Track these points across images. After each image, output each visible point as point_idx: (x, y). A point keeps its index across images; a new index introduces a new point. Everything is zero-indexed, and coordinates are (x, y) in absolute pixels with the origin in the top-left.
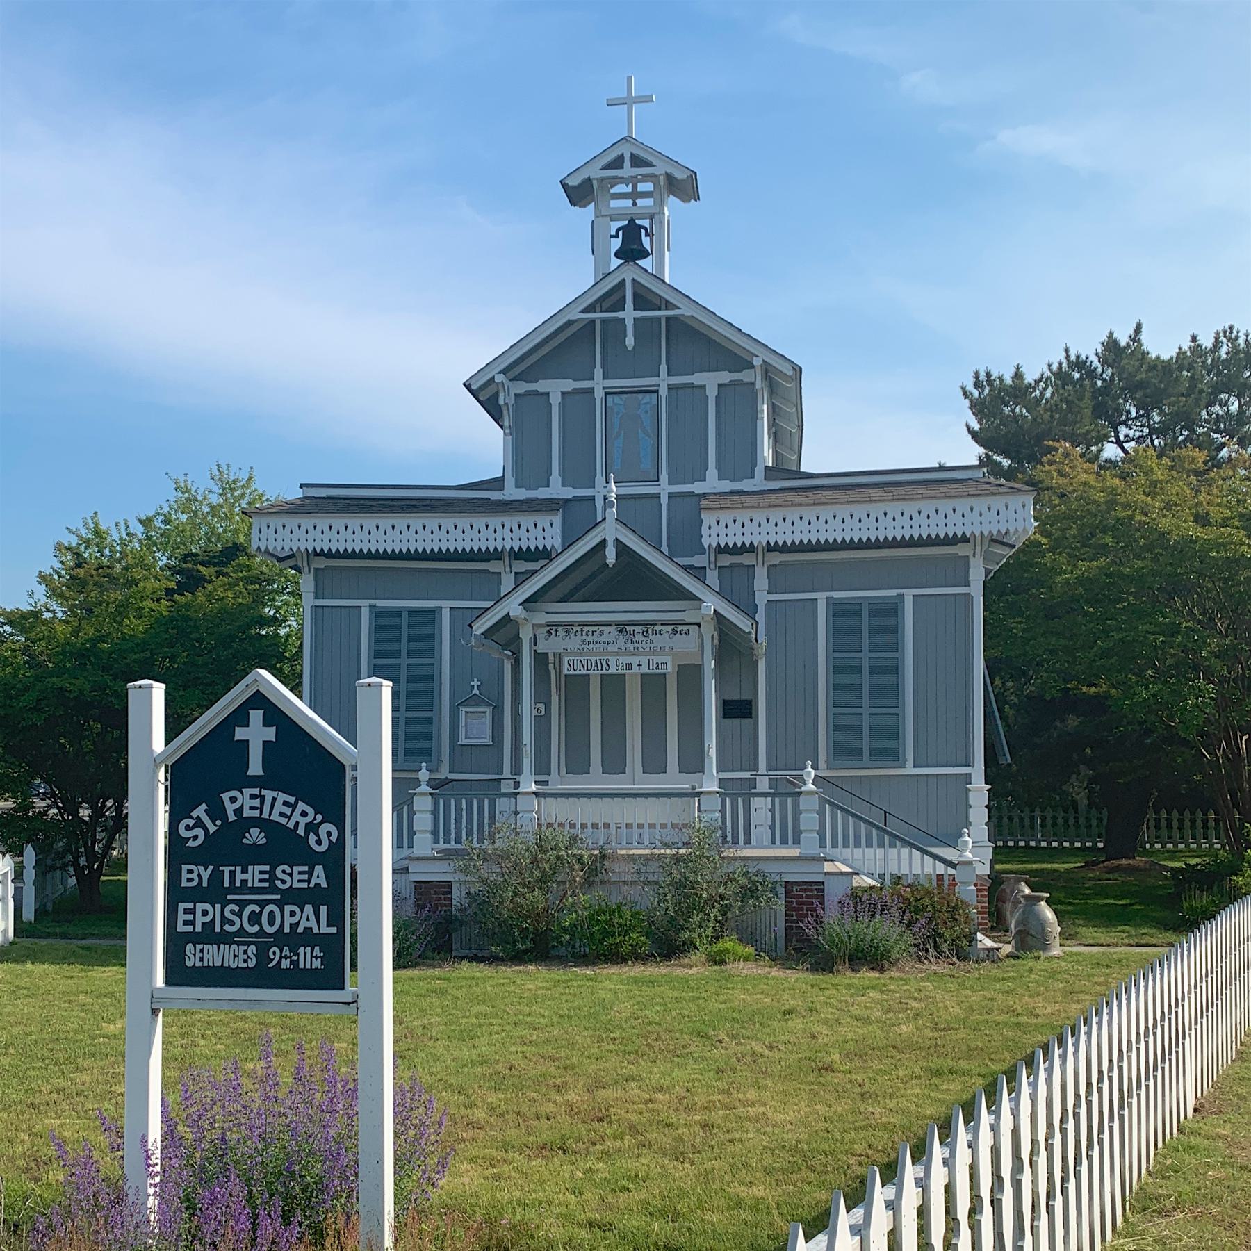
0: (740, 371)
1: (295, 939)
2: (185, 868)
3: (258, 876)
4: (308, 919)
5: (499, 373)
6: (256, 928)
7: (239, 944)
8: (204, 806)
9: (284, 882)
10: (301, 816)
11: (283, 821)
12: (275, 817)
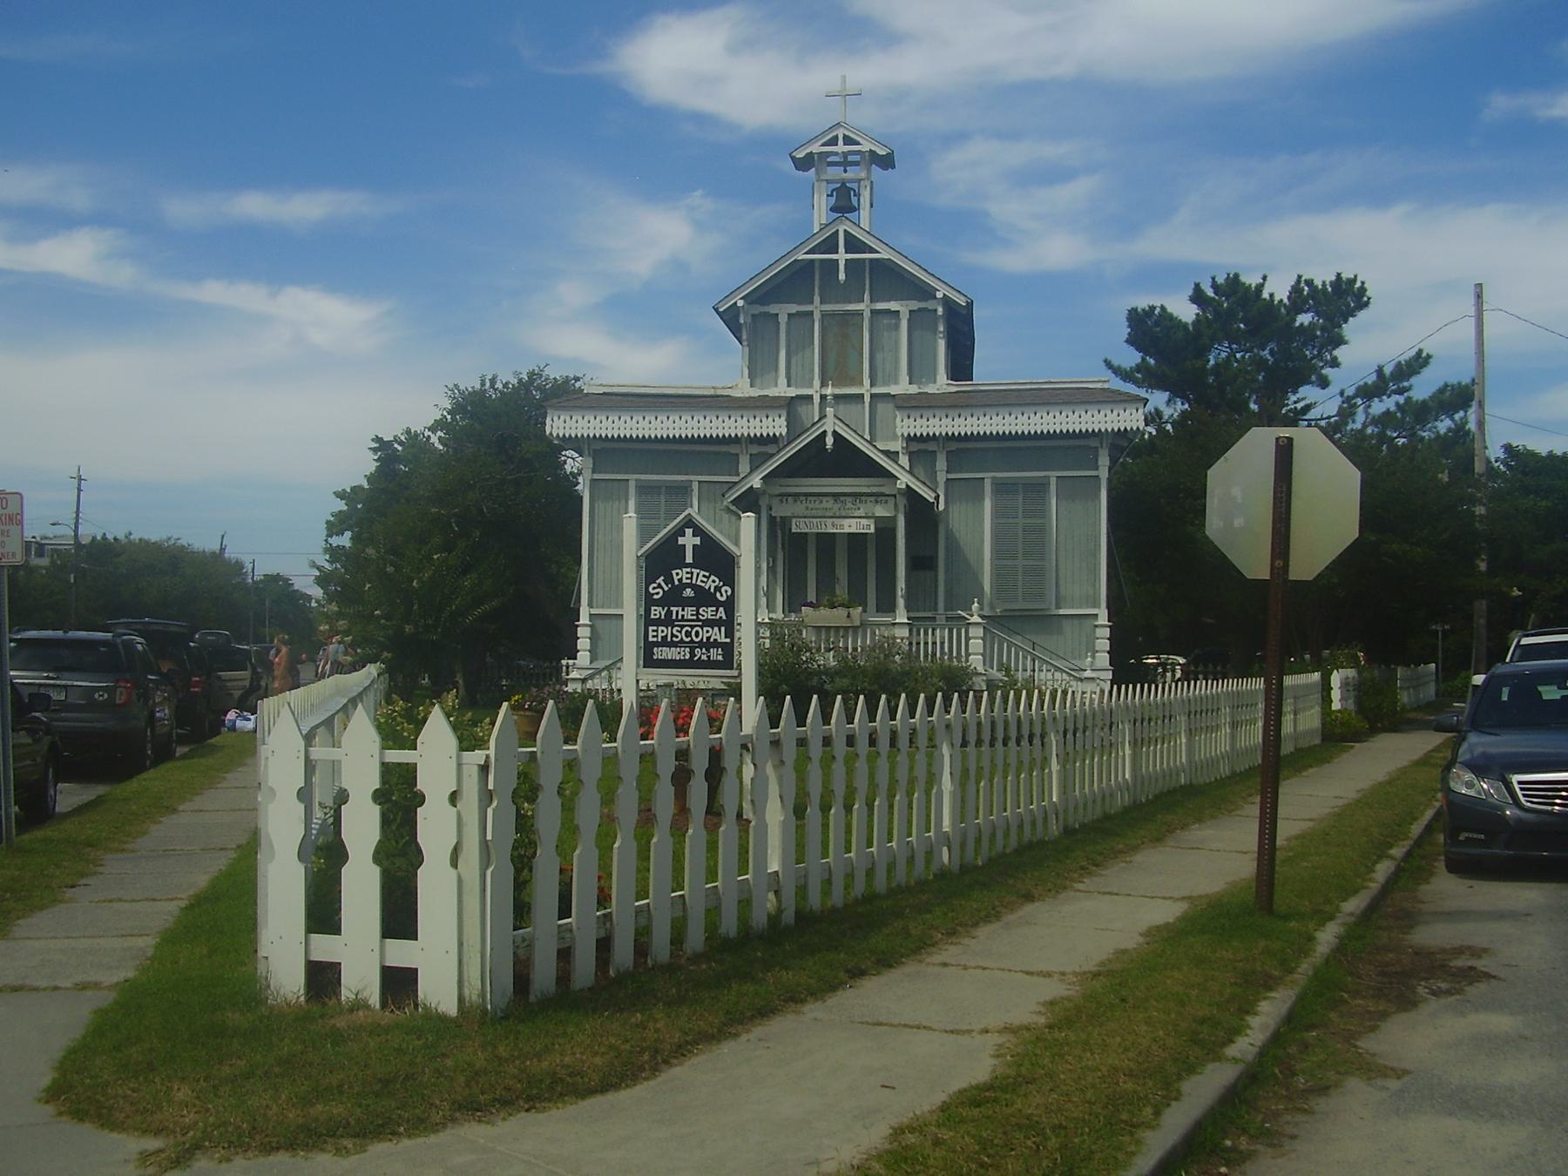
0: (927, 300)
1: (709, 644)
2: (653, 608)
3: (690, 613)
4: (718, 635)
5: (741, 299)
6: (689, 639)
7: (680, 647)
8: (662, 578)
9: (703, 616)
10: (712, 583)
11: (703, 585)
12: (699, 583)
